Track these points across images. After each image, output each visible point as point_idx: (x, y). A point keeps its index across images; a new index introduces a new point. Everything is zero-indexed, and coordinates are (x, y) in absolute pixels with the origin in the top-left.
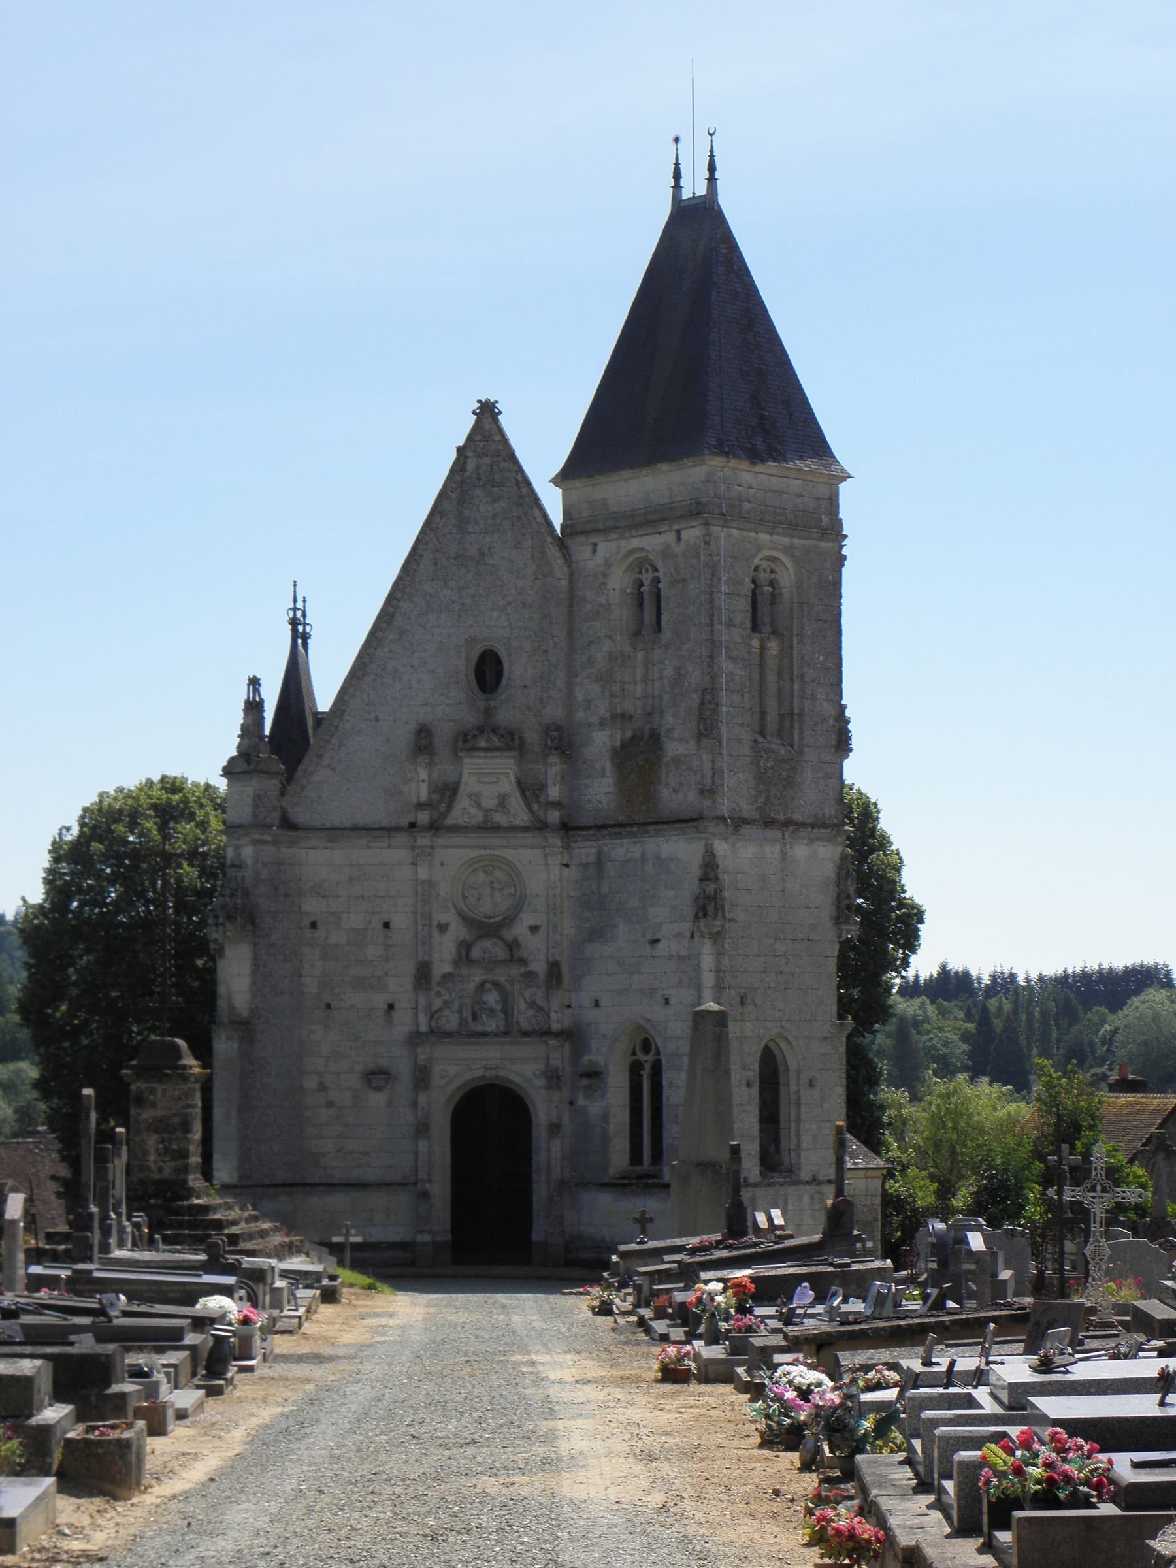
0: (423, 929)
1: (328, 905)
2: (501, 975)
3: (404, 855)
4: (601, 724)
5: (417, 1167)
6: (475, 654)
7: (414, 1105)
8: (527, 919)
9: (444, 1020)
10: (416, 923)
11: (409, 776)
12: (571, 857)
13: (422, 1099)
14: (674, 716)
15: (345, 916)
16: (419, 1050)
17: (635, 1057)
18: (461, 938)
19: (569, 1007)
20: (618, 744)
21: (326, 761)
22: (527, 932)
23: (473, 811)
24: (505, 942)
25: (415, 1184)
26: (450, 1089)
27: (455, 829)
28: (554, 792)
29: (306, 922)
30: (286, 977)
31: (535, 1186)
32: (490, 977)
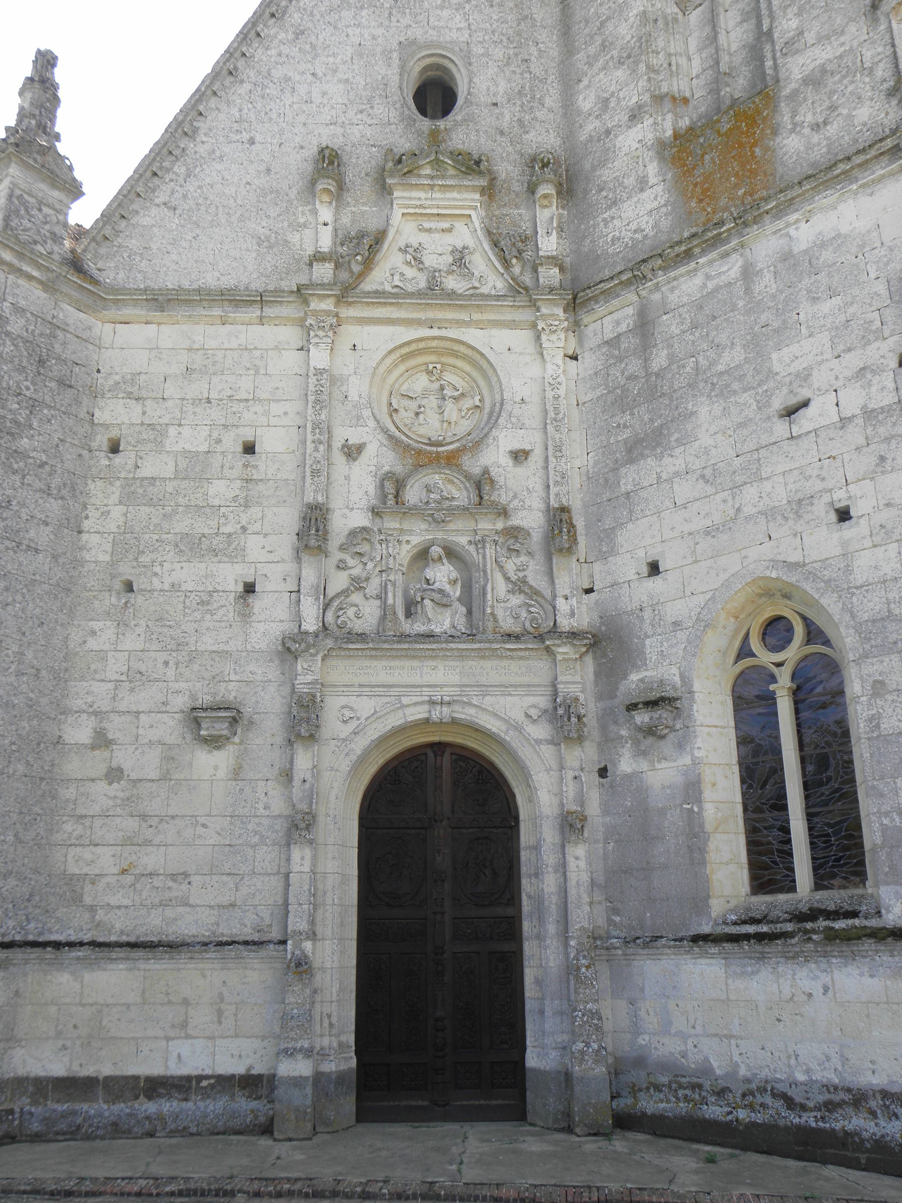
0: (316, 450)
1: (144, 413)
3: (290, 335)
5: (286, 904)
6: (415, 69)
7: (287, 776)
9: (351, 612)
10: (304, 442)
11: (302, 220)
12: (580, 342)
13: (303, 761)
15: (172, 431)
17: (748, 662)
18: (387, 468)
19: (589, 591)
20: (669, 133)
21: (161, 197)
22: (506, 461)
23: (410, 272)
24: (468, 476)
25: (284, 942)
26: (360, 745)
27: (380, 297)
28: (549, 244)
29: (101, 440)
30: (47, 524)
31: (529, 948)
32: (439, 535)
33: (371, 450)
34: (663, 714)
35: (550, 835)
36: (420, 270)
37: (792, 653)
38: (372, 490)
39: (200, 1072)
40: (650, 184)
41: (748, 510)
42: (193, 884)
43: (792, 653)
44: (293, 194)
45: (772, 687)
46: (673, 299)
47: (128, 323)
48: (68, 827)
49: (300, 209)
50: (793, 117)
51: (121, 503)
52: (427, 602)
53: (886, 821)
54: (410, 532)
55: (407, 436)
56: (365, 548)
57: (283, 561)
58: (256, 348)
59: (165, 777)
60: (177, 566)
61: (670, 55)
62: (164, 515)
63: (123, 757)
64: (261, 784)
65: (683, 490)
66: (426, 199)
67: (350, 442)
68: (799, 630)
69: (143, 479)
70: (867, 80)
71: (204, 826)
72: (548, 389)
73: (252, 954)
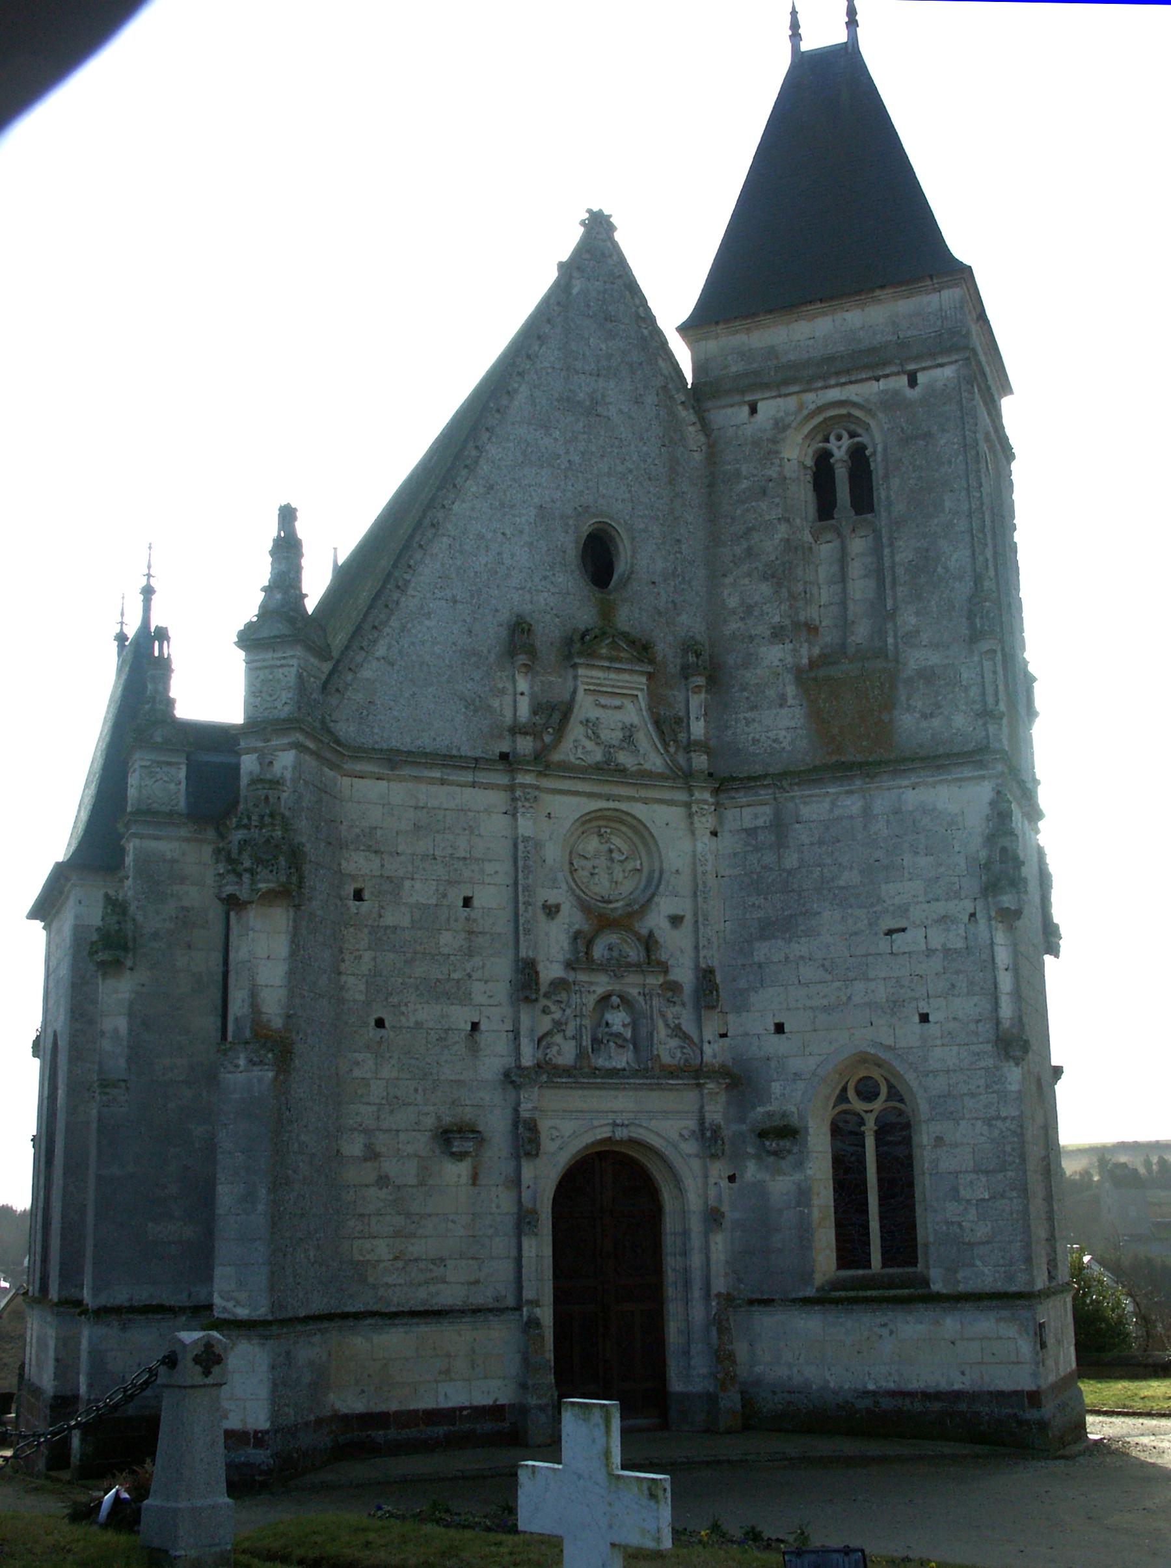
0: (526, 911)
1: (382, 866)
2: (632, 984)
3: (498, 799)
4: (775, 635)
6: (585, 530)
7: (516, 1182)
8: (665, 906)
9: (555, 1049)
11: (500, 686)
13: (528, 1171)
14: (917, 614)
15: (407, 883)
16: (523, 1095)
17: (844, 1106)
18: (577, 926)
20: (805, 661)
21: (381, 650)
22: (665, 924)
23: (590, 745)
25: (518, 1308)
27: (568, 770)
28: (698, 729)
29: (350, 889)
32: (617, 987)
33: (565, 909)
34: (786, 1143)
35: (696, 1225)
36: (597, 744)
37: (878, 1105)
38: (566, 945)
39: (461, 1405)
40: (789, 704)
41: (857, 999)
42: (449, 1267)
43: (878, 1105)
44: (492, 658)
45: (863, 1128)
46: (806, 811)
47: (362, 778)
48: (351, 1223)
49: (499, 674)
50: (908, 699)
51: (370, 948)
52: (611, 1044)
53: (937, 1227)
54: (597, 984)
55: (584, 893)
56: (563, 996)
57: (500, 1005)
58: (469, 810)
59: (422, 1184)
60: (419, 1006)
61: (805, 583)
62: (405, 962)
63: (390, 1167)
64: (494, 1189)
65: (808, 972)
66: (605, 679)
67: (549, 903)
68: (884, 1090)
69: (387, 927)
70: (963, 695)
71: (453, 1222)
72: (698, 865)
73: (496, 1319)
